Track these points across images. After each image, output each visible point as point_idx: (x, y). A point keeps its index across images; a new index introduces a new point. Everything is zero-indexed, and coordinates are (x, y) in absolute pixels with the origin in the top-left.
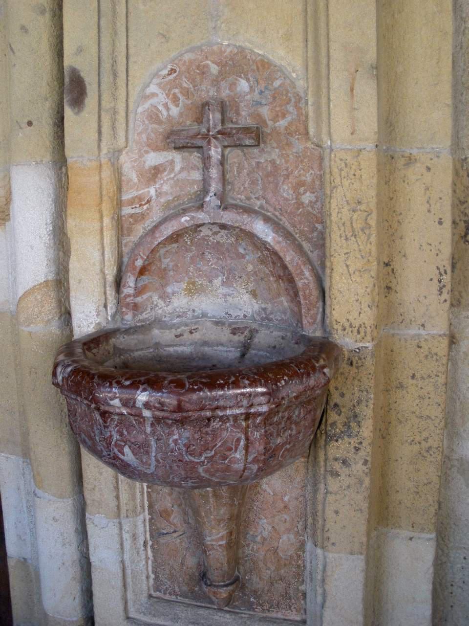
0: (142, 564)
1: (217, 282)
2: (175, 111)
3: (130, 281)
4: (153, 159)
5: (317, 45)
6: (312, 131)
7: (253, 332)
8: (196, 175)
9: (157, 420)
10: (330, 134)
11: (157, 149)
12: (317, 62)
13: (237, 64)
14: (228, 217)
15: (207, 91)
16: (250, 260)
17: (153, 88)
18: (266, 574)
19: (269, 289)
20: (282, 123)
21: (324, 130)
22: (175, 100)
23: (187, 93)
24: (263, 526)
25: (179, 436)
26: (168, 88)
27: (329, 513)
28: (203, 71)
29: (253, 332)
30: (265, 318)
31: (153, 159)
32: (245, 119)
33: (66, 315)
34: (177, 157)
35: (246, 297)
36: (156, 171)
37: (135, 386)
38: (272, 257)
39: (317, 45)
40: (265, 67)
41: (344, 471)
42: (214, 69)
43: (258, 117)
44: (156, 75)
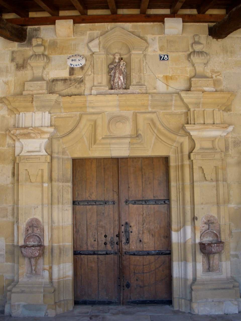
0: (202, 268)
1: (208, 237)
2: (205, 221)
3: (202, 237)
4: (203, 225)
5: (219, 215)
6: (218, 222)
7: (212, 242)
8: (208, 227)
9: (216, 246)
10: (221, 223)
11: (204, 224)
12: (219, 216)
13: (211, 216)
14: (212, 231)
15: (209, 219)
16: (213, 234)
17: (203, 218)
18: (215, 267)
19: (136, 228)
20: (216, 222)
21: (220, 222)
22: (206, 220)
23: (207, 219)
24: (215, 261)
25: (217, 248)
26: (205, 218)
27: (222, 258)
28: (208, 217)
29: (212, 242)
30: (213, 240)
31: (203, 225)
32: (212, 222)
33: (195, 241)
34: (206, 225)
35: (211, 238)
36: (203, 227)
37: (215, 244)
38: (216, 234)
39: (219, 215)
40: (214, 217)
41: (223, 253)
42: (209, 217)
43: (213, 221)
44: (203, 217)
